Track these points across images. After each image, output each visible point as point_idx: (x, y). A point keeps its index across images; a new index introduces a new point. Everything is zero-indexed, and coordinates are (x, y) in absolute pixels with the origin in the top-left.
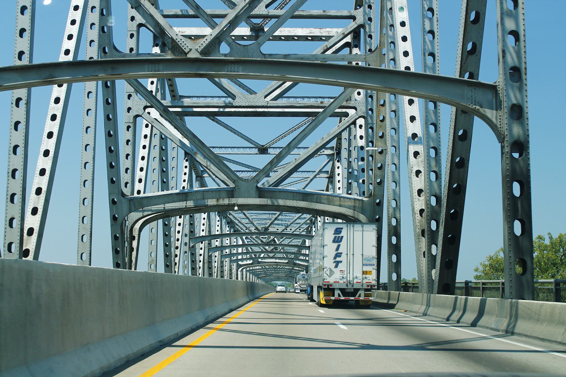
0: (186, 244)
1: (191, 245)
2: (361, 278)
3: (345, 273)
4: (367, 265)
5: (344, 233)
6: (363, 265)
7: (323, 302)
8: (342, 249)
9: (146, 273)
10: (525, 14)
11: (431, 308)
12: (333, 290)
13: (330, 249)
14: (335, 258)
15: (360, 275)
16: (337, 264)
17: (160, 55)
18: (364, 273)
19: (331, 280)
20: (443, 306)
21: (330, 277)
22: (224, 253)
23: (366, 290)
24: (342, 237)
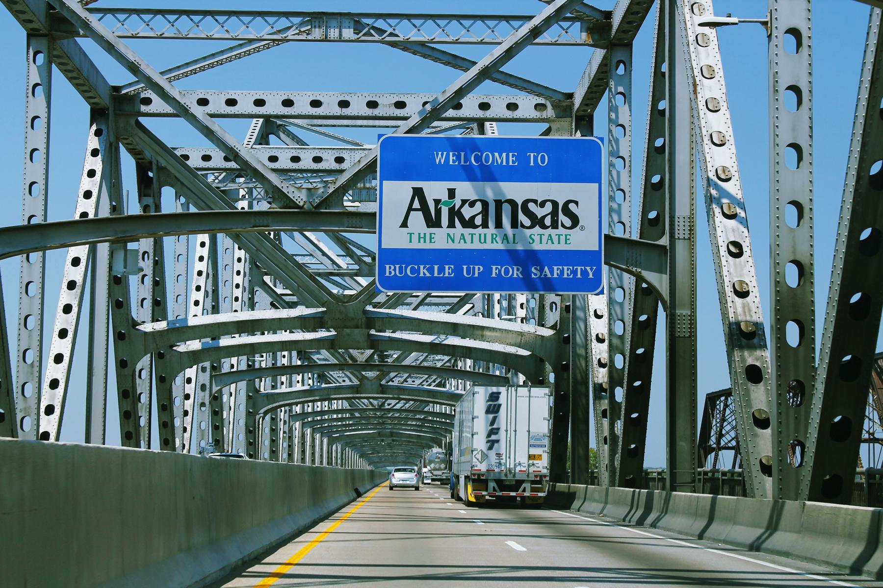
0: (203, 387)
1: (215, 389)
2: (526, 465)
3: (504, 457)
4: (534, 446)
5: (502, 400)
6: (530, 446)
7: (472, 499)
8: (502, 422)
9: (76, 447)
10: (813, 47)
11: (608, 506)
12: (486, 482)
13: (481, 425)
14: (489, 435)
15: (524, 460)
16: (492, 444)
17: (282, 230)
18: (530, 457)
19: (483, 467)
20: (618, 503)
21: (481, 463)
22: (226, 369)
23: (533, 482)
24: (500, 405)
